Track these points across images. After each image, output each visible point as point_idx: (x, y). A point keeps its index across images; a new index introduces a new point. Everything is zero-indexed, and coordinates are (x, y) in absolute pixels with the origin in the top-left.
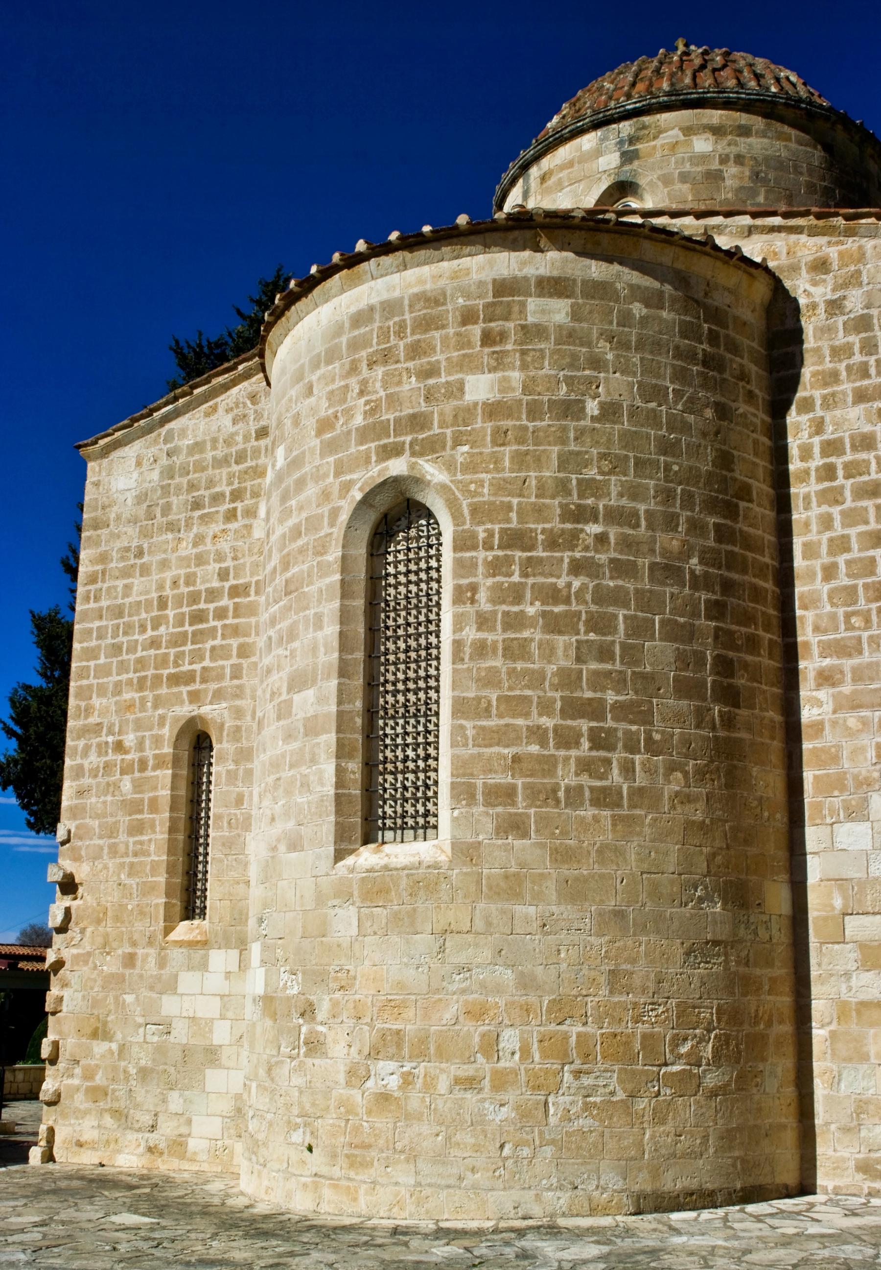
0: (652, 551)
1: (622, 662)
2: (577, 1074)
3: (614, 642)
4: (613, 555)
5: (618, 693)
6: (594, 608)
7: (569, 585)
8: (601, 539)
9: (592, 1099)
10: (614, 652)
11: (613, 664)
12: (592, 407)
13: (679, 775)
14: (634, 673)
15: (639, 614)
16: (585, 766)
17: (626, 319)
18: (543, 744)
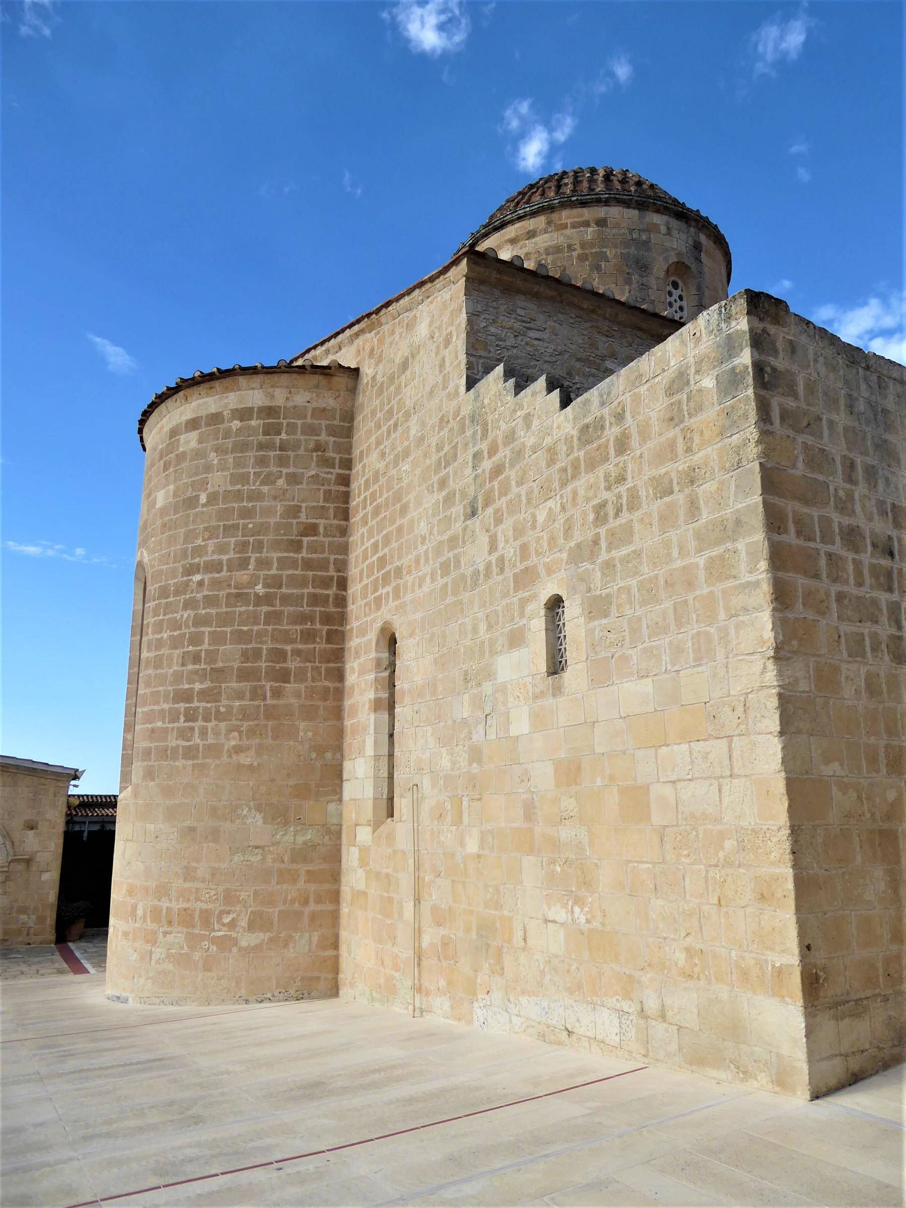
2: (165, 934)
3: (201, 650)
4: (206, 593)
5: (202, 683)
6: (193, 629)
7: (182, 616)
8: (201, 584)
9: (171, 951)
12: (203, 499)
13: (236, 734)
14: (211, 668)
15: (218, 629)
16: (183, 734)
18: (164, 723)
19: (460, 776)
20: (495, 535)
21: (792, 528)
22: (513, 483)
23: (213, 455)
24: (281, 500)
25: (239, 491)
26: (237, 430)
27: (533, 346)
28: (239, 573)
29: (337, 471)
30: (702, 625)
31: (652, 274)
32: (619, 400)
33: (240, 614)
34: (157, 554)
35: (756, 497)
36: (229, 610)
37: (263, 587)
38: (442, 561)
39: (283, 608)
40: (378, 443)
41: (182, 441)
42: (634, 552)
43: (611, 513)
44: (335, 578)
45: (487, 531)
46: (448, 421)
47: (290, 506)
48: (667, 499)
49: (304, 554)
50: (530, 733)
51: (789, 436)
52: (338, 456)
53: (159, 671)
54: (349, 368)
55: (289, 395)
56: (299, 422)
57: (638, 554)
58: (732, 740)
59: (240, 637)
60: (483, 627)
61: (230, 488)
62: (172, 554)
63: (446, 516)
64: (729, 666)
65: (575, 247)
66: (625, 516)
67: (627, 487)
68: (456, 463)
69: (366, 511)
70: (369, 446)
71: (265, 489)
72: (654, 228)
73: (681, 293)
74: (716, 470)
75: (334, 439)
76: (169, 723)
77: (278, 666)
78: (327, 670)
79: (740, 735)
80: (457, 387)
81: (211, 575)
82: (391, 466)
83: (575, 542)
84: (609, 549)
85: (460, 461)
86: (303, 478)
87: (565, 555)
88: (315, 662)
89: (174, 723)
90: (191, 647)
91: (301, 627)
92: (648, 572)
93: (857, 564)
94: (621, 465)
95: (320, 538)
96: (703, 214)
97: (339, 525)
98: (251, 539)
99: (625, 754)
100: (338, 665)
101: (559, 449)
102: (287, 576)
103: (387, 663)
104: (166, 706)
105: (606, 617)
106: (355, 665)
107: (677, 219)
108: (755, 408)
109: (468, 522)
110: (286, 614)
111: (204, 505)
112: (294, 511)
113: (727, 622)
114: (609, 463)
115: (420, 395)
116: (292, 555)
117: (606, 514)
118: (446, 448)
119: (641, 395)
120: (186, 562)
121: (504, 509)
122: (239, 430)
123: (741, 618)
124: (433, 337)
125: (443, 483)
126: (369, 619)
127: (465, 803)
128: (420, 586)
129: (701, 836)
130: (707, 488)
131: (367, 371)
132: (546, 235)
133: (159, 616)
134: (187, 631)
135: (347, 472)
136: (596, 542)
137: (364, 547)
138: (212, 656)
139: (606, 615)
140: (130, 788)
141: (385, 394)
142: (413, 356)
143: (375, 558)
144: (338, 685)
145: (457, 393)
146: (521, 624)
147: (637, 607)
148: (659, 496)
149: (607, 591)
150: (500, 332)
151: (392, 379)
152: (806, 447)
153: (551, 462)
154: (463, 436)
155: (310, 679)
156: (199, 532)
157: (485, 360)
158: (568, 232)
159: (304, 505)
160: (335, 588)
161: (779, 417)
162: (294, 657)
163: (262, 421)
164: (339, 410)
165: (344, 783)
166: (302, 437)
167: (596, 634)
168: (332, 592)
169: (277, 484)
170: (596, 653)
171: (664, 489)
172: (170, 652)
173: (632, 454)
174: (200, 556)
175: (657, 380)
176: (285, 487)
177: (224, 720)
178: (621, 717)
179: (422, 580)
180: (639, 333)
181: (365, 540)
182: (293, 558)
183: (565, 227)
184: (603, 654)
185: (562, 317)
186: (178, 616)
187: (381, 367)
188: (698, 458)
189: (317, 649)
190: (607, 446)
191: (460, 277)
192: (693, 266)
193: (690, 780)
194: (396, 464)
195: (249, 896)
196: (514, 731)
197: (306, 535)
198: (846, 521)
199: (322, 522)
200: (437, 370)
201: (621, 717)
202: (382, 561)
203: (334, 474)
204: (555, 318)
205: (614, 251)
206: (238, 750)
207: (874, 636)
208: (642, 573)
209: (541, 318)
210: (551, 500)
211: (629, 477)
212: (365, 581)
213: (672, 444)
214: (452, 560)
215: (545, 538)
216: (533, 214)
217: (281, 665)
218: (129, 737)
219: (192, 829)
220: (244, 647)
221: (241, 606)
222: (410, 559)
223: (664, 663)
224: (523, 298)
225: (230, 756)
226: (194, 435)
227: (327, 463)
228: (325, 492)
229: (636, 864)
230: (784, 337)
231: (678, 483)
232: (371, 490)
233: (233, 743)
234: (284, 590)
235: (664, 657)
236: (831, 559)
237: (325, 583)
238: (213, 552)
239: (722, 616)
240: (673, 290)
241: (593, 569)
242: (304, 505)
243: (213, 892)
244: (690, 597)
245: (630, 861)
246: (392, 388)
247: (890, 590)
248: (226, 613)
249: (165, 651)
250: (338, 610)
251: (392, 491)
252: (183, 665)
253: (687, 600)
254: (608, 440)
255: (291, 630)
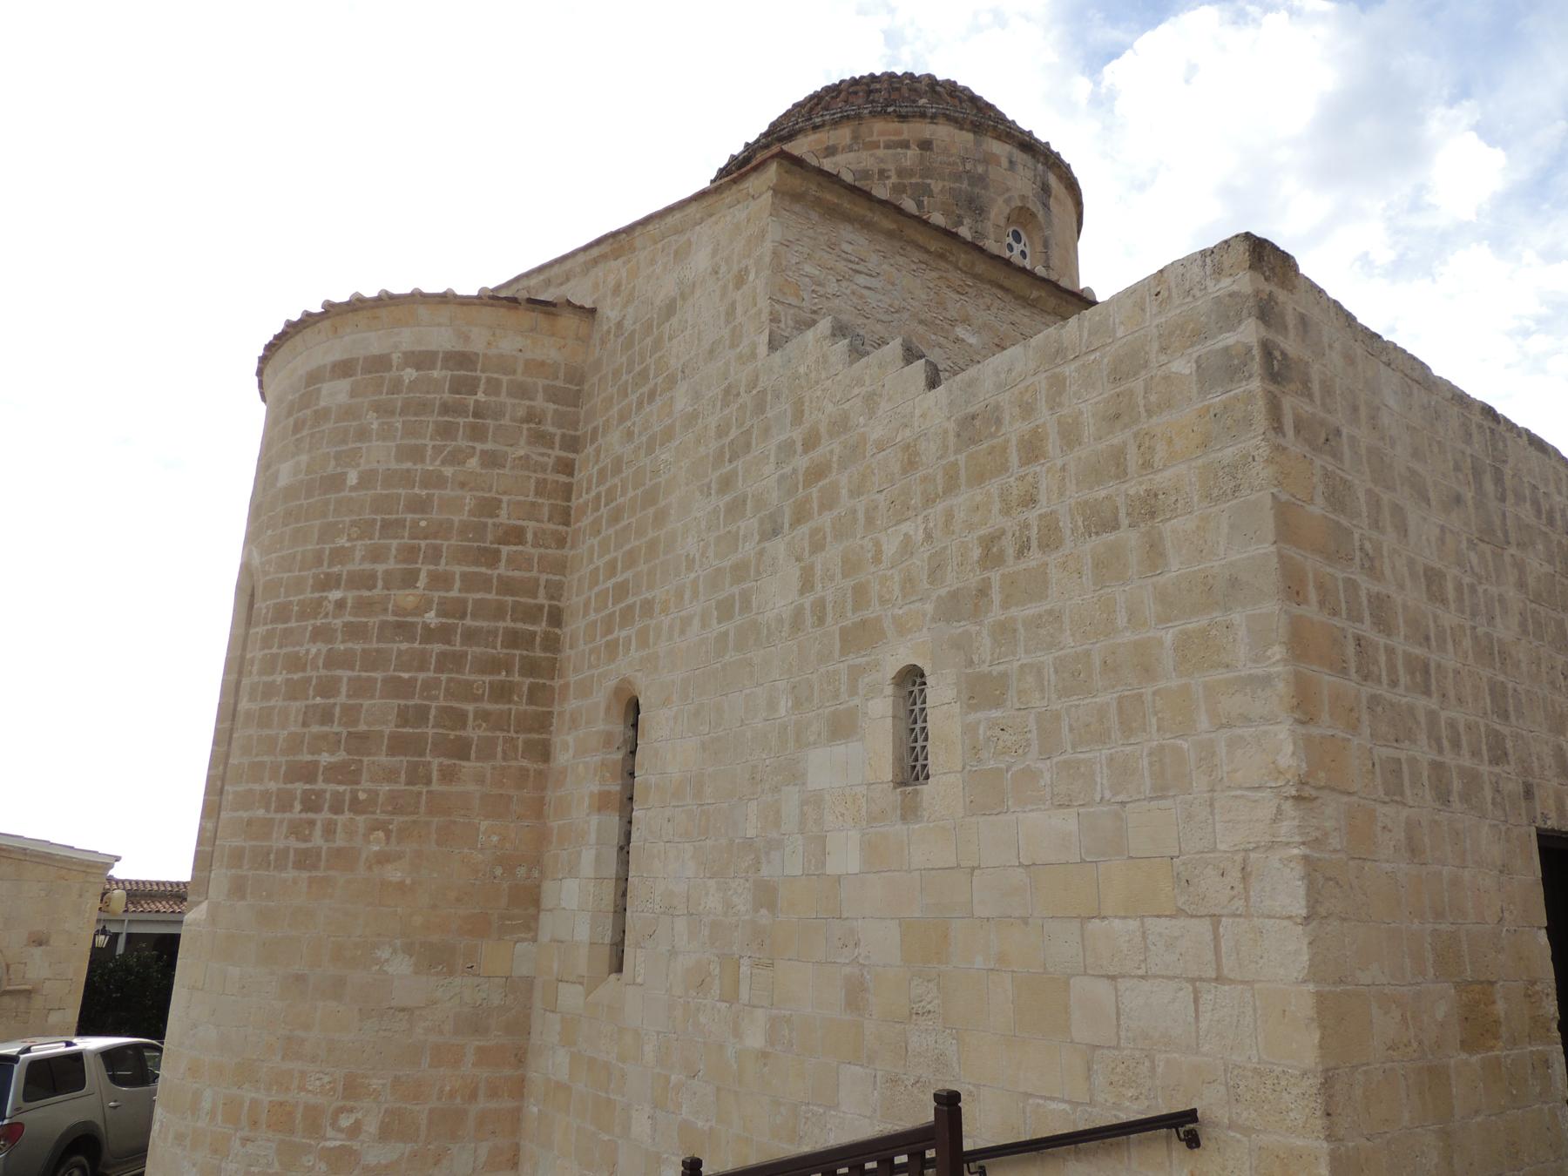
0: (385, 610)
1: (339, 724)
2: (245, 1140)
3: (335, 704)
4: (348, 618)
5: (332, 754)
6: (323, 672)
7: (308, 651)
8: (340, 604)
9: (252, 1169)
10: (334, 715)
11: (332, 726)
12: (352, 478)
13: (381, 834)
16: (296, 830)
17: (396, 386)
18: (268, 810)
19: (737, 926)
20: (812, 567)
21: (1313, 595)
22: (844, 492)
23: (372, 415)
24: (471, 490)
25: (408, 471)
26: (411, 382)
27: (861, 297)
28: (401, 592)
29: (557, 452)
30: (1168, 735)
31: (989, 219)
32: (1027, 383)
33: (400, 653)
34: (274, 555)
35: (1267, 545)
36: (382, 645)
37: (438, 615)
38: (720, 598)
39: (465, 648)
40: (623, 418)
41: (324, 392)
42: (1050, 612)
43: (1011, 552)
44: (546, 610)
45: (798, 560)
46: (738, 394)
47: (485, 499)
48: (1110, 537)
49: (502, 569)
50: (860, 873)
51: (1305, 456)
52: (559, 432)
53: (266, 732)
54: (582, 307)
55: (492, 338)
56: (505, 379)
57: (1056, 616)
58: (1219, 922)
59: (399, 688)
60: (784, 705)
61: (394, 465)
62: (299, 557)
63: (729, 532)
64: (1217, 805)
65: (889, 173)
66: (1034, 558)
67: (1039, 512)
68: (748, 457)
69: (599, 513)
70: (608, 420)
71: (448, 471)
72: (989, 159)
73: (1023, 248)
74: (1196, 499)
75: (556, 407)
76: (276, 812)
77: (452, 735)
78: (526, 742)
79: (1235, 915)
80: (754, 346)
81: (356, 593)
82: (643, 452)
83: (947, 589)
84: (1005, 605)
85: (756, 453)
86: (506, 460)
87: (929, 608)
88: (509, 732)
89: (284, 812)
90: (318, 698)
91: (492, 678)
92: (1072, 645)
93: (1390, 651)
94: (1030, 478)
95: (528, 549)
96: (1054, 148)
97: (557, 531)
98: (423, 543)
99: (1026, 924)
100: (544, 736)
101: (923, 448)
102: (476, 602)
103: (621, 740)
104: (273, 786)
105: (997, 706)
106: (570, 739)
107: (1021, 151)
108: (1263, 410)
109: (766, 544)
110: (469, 657)
111: (353, 489)
112: (489, 507)
113: (1213, 735)
114: (1008, 474)
115: (693, 353)
116: (483, 570)
117: (1002, 551)
118: (734, 433)
119: (1065, 379)
120: (320, 570)
121: (828, 530)
122: (414, 384)
123: (1239, 731)
124: (716, 273)
125: (726, 483)
126: (596, 672)
127: (745, 969)
128: (683, 632)
129: (1160, 1070)
130: (1174, 528)
131: (610, 313)
132: (852, 154)
133: (271, 648)
134: (314, 674)
135: (572, 456)
136: (983, 591)
137: (592, 567)
138: (351, 713)
139: (998, 703)
140: (204, 906)
141: (637, 348)
142: (683, 297)
143: (610, 584)
144: (541, 766)
145: (753, 355)
146: (852, 704)
147: (1054, 697)
148: (1094, 530)
149: (1002, 668)
150: (817, 273)
151: (648, 328)
152: (1327, 475)
153: (911, 464)
154: (762, 417)
155: (499, 755)
156: (344, 528)
157: (796, 309)
158: (881, 152)
159: (505, 498)
160: (544, 624)
161: (1292, 429)
162: (477, 723)
163: (450, 373)
164: (563, 366)
165: (542, 915)
166: (509, 401)
167: (981, 731)
168: (540, 628)
169: (467, 465)
170: (979, 760)
171: (1101, 521)
172: (286, 703)
173: (1049, 464)
174: (342, 563)
175: (1092, 357)
176: (478, 470)
177: (363, 812)
178: (1021, 865)
179: (686, 622)
180: (1000, 293)
181: (596, 556)
182: (486, 574)
183: (876, 145)
184: (992, 764)
185: (901, 260)
186: (302, 651)
187: (631, 310)
188: (1162, 479)
189: (513, 712)
190: (1004, 449)
191: (765, 188)
192: (1040, 215)
193: (1142, 977)
194: (650, 450)
195: (384, 1085)
196: (832, 867)
197: (507, 543)
198: (1376, 588)
199: (531, 525)
200: (723, 318)
201: (1021, 865)
202: (622, 590)
203: (552, 457)
204: (892, 262)
205: (940, 184)
206: (383, 859)
207: (1413, 761)
208: (1062, 645)
209: (874, 259)
210: (908, 523)
211: (1043, 498)
212: (592, 616)
213: (1118, 456)
214: (737, 597)
215: (896, 578)
216: (836, 123)
217: (458, 733)
218: (210, 826)
219: (300, 979)
220: (402, 702)
221: (401, 642)
222: (668, 591)
223: (1099, 788)
224: (849, 228)
225: (370, 868)
226: (344, 385)
227: (541, 438)
228: (538, 482)
229: (1041, 1102)
230: (1295, 309)
231: (1128, 514)
232: (608, 484)
233: (376, 848)
234: (468, 622)
235: (1099, 780)
236: (1359, 645)
237: (532, 614)
238: (363, 559)
239: (1203, 722)
240: (1014, 244)
241: (978, 633)
242: (505, 498)
243: (326, 1079)
244: (1148, 691)
245: (1031, 1095)
246: (649, 340)
247: (1427, 692)
248: (378, 651)
249: (276, 702)
250: (548, 655)
251: (641, 489)
252: (305, 724)
253: (1141, 695)
254: (1007, 441)
255: (475, 681)
